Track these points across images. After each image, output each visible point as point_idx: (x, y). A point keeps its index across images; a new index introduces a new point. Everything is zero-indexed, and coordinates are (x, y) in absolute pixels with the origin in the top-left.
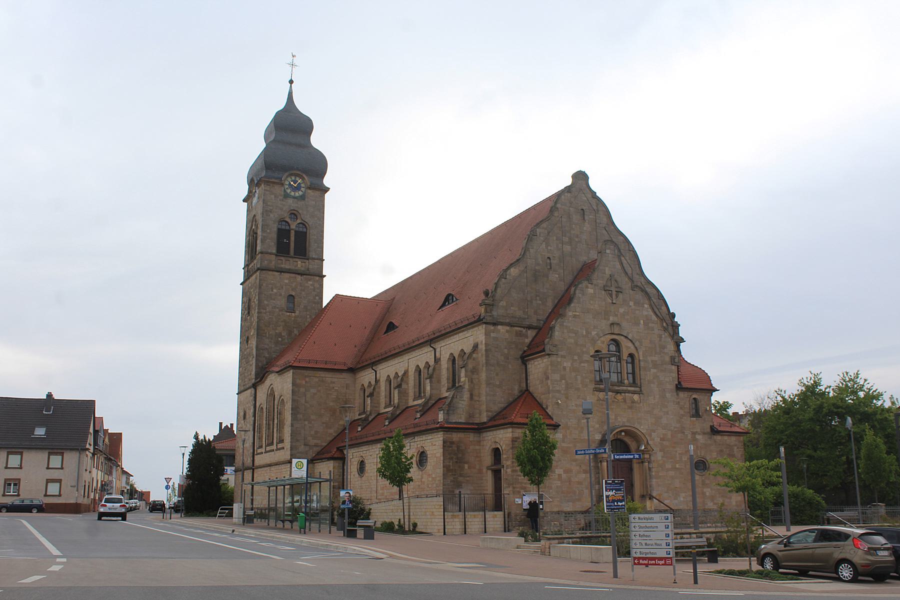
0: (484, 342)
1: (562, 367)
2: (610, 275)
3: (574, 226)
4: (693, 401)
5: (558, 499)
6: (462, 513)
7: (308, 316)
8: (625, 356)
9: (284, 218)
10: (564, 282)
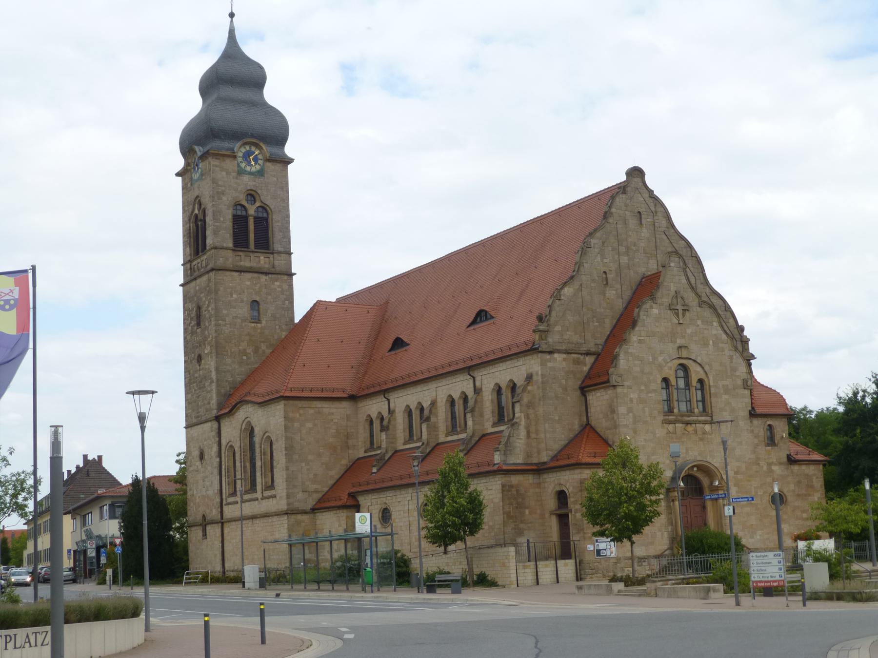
0: (540, 373)
2: (676, 291)
3: (630, 233)
4: (768, 428)
6: (532, 564)
7: (277, 327)
8: (694, 382)
10: (622, 299)
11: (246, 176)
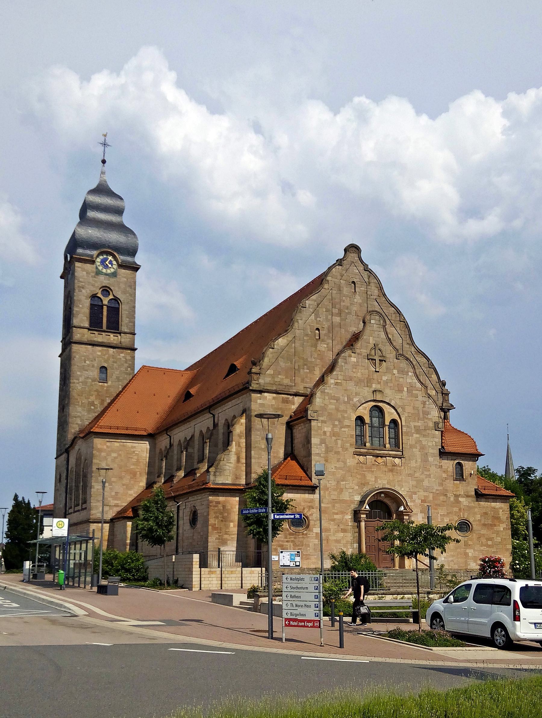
1: (322, 431)
2: (374, 344)
5: (316, 557)
9: (97, 294)
11: (103, 276)
